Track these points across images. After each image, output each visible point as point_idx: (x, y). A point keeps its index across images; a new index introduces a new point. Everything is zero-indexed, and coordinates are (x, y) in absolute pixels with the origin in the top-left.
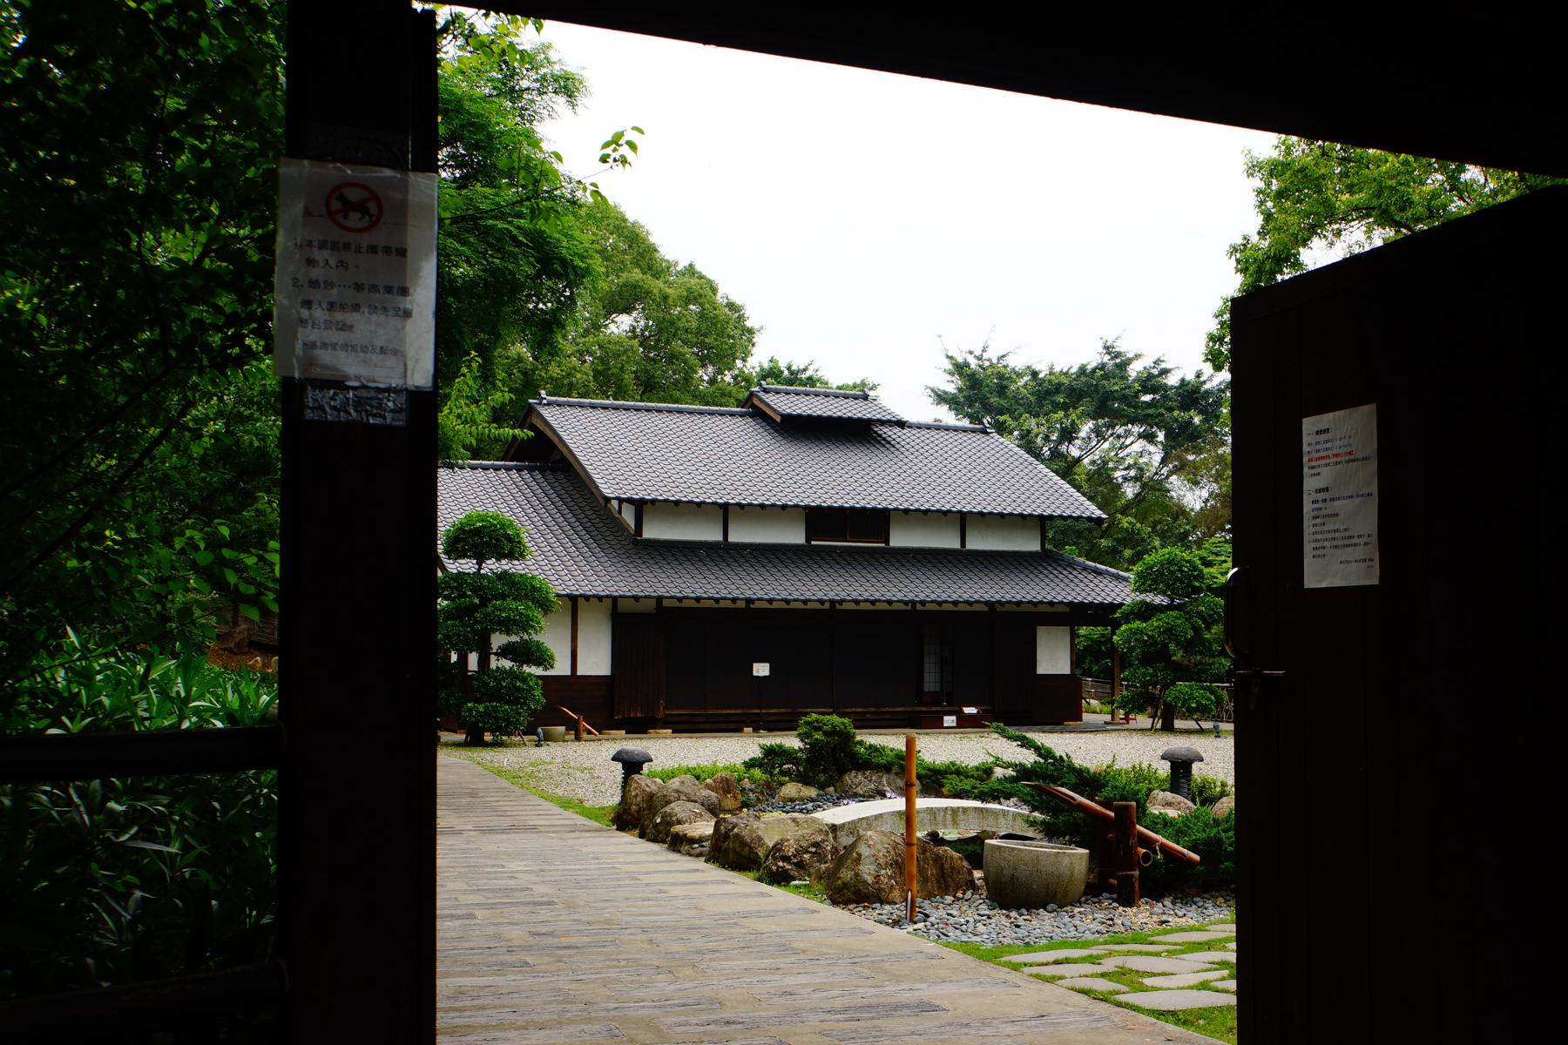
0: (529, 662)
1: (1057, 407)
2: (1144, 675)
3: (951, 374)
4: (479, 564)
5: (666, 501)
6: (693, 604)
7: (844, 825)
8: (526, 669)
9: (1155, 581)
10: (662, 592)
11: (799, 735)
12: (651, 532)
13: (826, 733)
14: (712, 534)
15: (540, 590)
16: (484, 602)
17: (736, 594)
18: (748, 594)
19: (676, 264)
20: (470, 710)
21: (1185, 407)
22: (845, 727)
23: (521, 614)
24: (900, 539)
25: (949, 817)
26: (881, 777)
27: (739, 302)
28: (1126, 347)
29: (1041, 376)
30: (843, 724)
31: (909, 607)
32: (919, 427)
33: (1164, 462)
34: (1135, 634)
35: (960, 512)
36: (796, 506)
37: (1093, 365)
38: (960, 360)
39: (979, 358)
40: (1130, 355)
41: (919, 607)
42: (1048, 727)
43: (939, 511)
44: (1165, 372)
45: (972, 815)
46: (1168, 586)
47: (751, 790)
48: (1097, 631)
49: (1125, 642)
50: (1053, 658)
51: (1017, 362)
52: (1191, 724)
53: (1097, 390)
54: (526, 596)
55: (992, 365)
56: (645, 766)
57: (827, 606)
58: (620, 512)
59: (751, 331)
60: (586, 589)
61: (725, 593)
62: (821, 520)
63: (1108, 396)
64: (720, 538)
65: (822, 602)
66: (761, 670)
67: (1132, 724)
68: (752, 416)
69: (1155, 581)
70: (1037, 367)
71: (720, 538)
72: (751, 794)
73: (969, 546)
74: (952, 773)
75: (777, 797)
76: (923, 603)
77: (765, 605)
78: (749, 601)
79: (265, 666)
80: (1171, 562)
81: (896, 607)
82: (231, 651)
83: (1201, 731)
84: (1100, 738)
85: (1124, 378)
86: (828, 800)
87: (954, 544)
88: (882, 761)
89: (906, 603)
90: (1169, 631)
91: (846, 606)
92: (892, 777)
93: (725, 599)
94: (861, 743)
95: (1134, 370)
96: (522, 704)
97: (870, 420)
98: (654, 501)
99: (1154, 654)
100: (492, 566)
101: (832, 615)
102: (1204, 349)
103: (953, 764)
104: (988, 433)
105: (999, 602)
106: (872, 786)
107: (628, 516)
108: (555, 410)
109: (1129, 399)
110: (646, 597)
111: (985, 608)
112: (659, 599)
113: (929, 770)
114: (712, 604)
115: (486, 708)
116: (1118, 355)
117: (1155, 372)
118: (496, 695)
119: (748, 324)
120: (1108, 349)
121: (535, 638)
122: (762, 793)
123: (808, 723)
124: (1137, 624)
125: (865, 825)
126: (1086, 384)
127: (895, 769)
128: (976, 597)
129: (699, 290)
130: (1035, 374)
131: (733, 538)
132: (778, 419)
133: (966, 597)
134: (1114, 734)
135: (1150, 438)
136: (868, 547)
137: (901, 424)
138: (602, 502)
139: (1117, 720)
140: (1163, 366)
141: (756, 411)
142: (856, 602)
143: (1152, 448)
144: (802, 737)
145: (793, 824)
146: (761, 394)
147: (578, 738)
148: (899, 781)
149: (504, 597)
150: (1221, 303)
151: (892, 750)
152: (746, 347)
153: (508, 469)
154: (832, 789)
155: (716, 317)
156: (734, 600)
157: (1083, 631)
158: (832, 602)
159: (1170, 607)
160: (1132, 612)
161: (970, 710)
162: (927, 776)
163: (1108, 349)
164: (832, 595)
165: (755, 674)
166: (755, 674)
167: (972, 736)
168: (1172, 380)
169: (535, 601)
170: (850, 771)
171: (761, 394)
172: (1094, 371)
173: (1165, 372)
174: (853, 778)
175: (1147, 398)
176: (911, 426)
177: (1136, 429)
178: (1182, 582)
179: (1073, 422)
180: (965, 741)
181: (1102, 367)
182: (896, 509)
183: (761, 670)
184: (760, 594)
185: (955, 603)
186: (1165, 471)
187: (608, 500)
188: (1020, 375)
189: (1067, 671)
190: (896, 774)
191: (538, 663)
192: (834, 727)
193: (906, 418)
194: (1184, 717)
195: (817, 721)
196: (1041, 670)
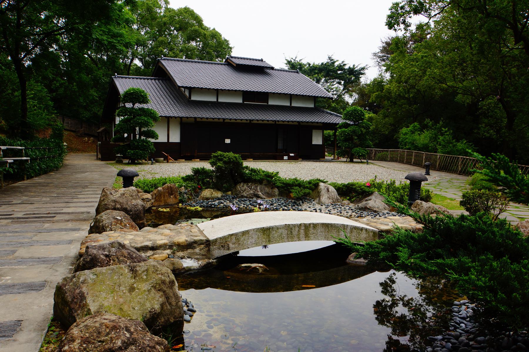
0: (149, 137)
1: (315, 73)
2: (346, 145)
3: (286, 64)
4: (134, 105)
5: (198, 88)
6: (206, 120)
7: (216, 240)
8: (150, 139)
9: (350, 116)
10: (196, 116)
11: (211, 163)
12: (194, 98)
13: (225, 163)
14: (213, 99)
15: (153, 113)
16: (134, 117)
17: (220, 117)
18: (223, 117)
19: (210, 28)
20: (129, 152)
21: (350, 74)
22: (236, 159)
23: (145, 121)
24: (271, 102)
25: (302, 231)
26: (257, 187)
27: (227, 39)
28: (335, 58)
29: (311, 66)
30: (235, 157)
31: (274, 123)
32: (278, 70)
33: (344, 90)
34: (343, 132)
35: (290, 94)
36: (239, 90)
37: (325, 62)
38: (289, 60)
39: (294, 60)
40: (335, 60)
41: (277, 123)
42: (315, 160)
43: (284, 93)
44: (345, 65)
45: (320, 229)
46: (354, 118)
47: (185, 193)
48: (331, 132)
49: (340, 135)
50: (317, 140)
51: (304, 62)
52: (359, 160)
53: (326, 69)
54: (149, 116)
55: (298, 62)
56: (136, 180)
57: (248, 122)
58: (185, 92)
59: (231, 48)
60: (172, 115)
61: (216, 117)
62: (247, 95)
63: (330, 71)
64: (215, 100)
65: (247, 120)
66: (228, 141)
67: (340, 160)
68: (227, 65)
69: (350, 116)
70: (309, 62)
71: (215, 100)
72: (185, 195)
73: (292, 105)
74: (296, 186)
75: (199, 197)
76: (278, 121)
77: (229, 121)
78: (224, 119)
79: (89, 140)
80: (355, 110)
81: (270, 122)
82: (79, 136)
83: (362, 162)
84: (332, 164)
85: (334, 66)
86: (227, 199)
87: (288, 104)
88: (257, 178)
89: (273, 121)
90: (354, 132)
91: (254, 122)
92: (263, 186)
93: (216, 118)
94: (247, 168)
95: (336, 64)
96: (146, 151)
97: (263, 67)
98: (194, 88)
99: (348, 138)
100: (137, 106)
101: (250, 125)
102: (386, 21)
103: (296, 179)
104: (299, 73)
105: (302, 122)
106: (252, 192)
107: (187, 93)
108: (166, 61)
109: (335, 71)
110: (190, 117)
111: (297, 124)
112: (195, 118)
113: (283, 183)
114: (212, 120)
115: (134, 151)
116: (332, 60)
117: (342, 65)
118: (137, 148)
119: (230, 46)
120: (329, 58)
121: (152, 129)
122: (191, 195)
123: (215, 156)
124: (344, 129)
125: (234, 240)
126: (324, 67)
127: (265, 182)
128: (295, 120)
129: (215, 35)
130: (309, 64)
131: (220, 100)
132: (235, 65)
133: (291, 120)
134: (336, 163)
135: (339, 83)
136: (310, 285)
137: (272, 68)
138: (178, 88)
139: (335, 159)
140: (344, 63)
141: (229, 63)
142: (258, 120)
143: (340, 86)
144: (213, 164)
145: (130, 275)
146: (230, 58)
147: (168, 162)
148: (266, 189)
149: (141, 115)
150: (392, 5)
151: (263, 172)
152: (230, 52)
153: (151, 79)
154: (230, 193)
155: (220, 41)
156: (219, 119)
157: (325, 132)
158: (250, 120)
159: (355, 125)
160: (342, 126)
161: (292, 155)
162: (282, 187)
163: (329, 58)
164: (250, 118)
165: (226, 142)
166: (226, 142)
167: (293, 162)
168: (347, 67)
169: (151, 117)
170: (240, 183)
171: (230, 58)
172: (326, 64)
173: (345, 65)
174: (244, 189)
175: (339, 72)
176: (276, 70)
177: (337, 80)
178: (358, 117)
179: (320, 77)
180: (291, 164)
181: (328, 63)
182: (271, 93)
183: (228, 141)
184: (227, 117)
185: (288, 121)
186: (343, 92)
187: (179, 87)
188: (305, 65)
189: (321, 143)
190: (265, 185)
191: (153, 138)
192: (229, 159)
193: (273, 65)
194: (356, 158)
195: (221, 155)
196: (313, 143)
